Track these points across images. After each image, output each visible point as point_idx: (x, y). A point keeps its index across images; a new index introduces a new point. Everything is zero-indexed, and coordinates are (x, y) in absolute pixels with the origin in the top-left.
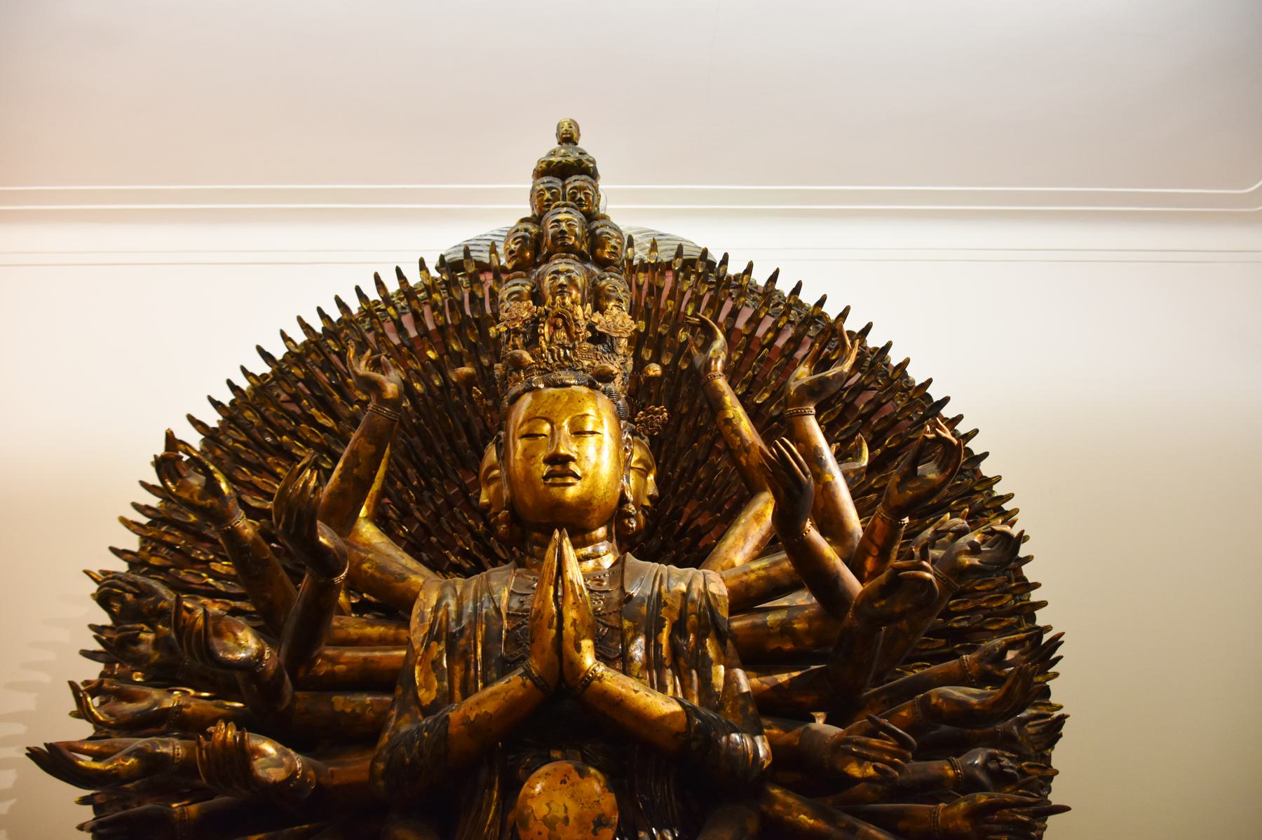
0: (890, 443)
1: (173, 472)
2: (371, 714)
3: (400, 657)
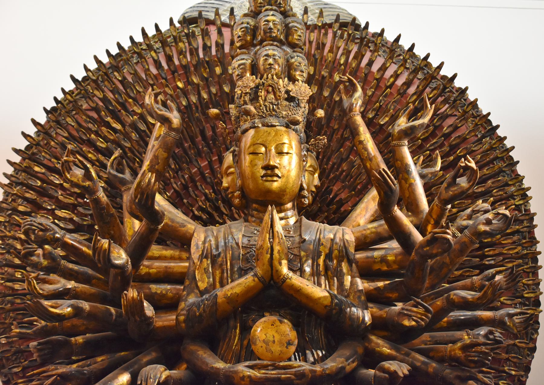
0: (460, 152)
1: (68, 168)
2: (171, 294)
3: (185, 267)
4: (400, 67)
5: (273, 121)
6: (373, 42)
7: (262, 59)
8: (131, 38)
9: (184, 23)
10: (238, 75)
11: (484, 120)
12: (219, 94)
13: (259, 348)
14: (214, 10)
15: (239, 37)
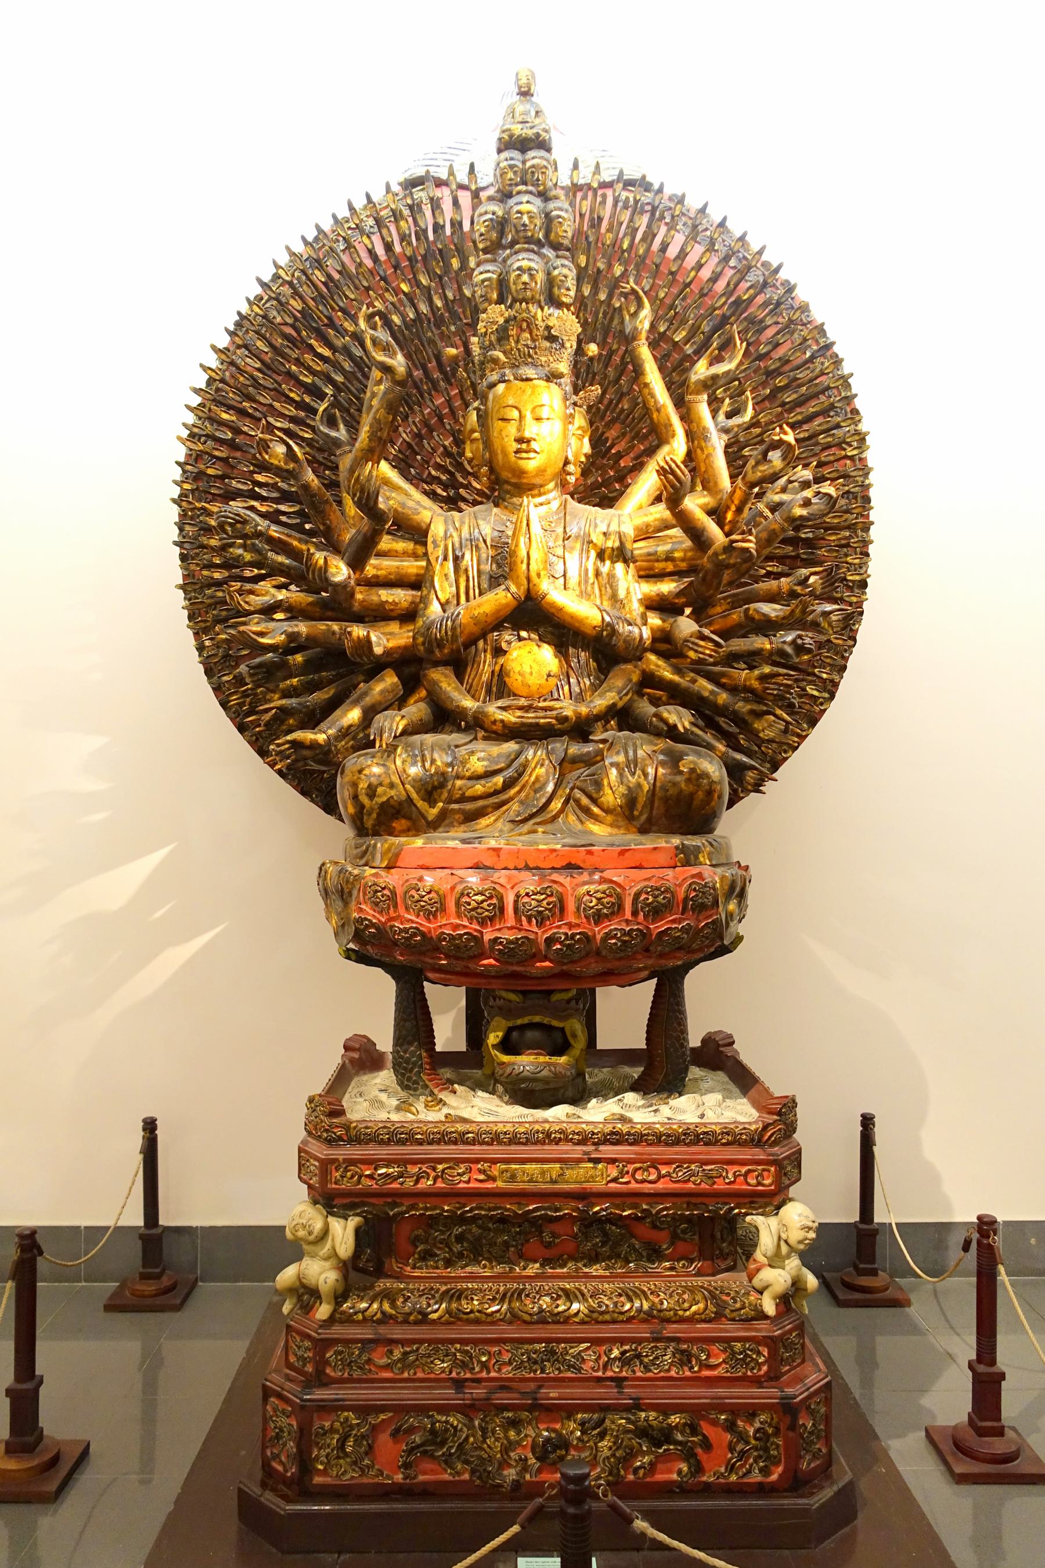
0: (780, 382)
3: (422, 567)
5: (529, 372)
7: (513, 275)
13: (514, 681)
15: (481, 235)
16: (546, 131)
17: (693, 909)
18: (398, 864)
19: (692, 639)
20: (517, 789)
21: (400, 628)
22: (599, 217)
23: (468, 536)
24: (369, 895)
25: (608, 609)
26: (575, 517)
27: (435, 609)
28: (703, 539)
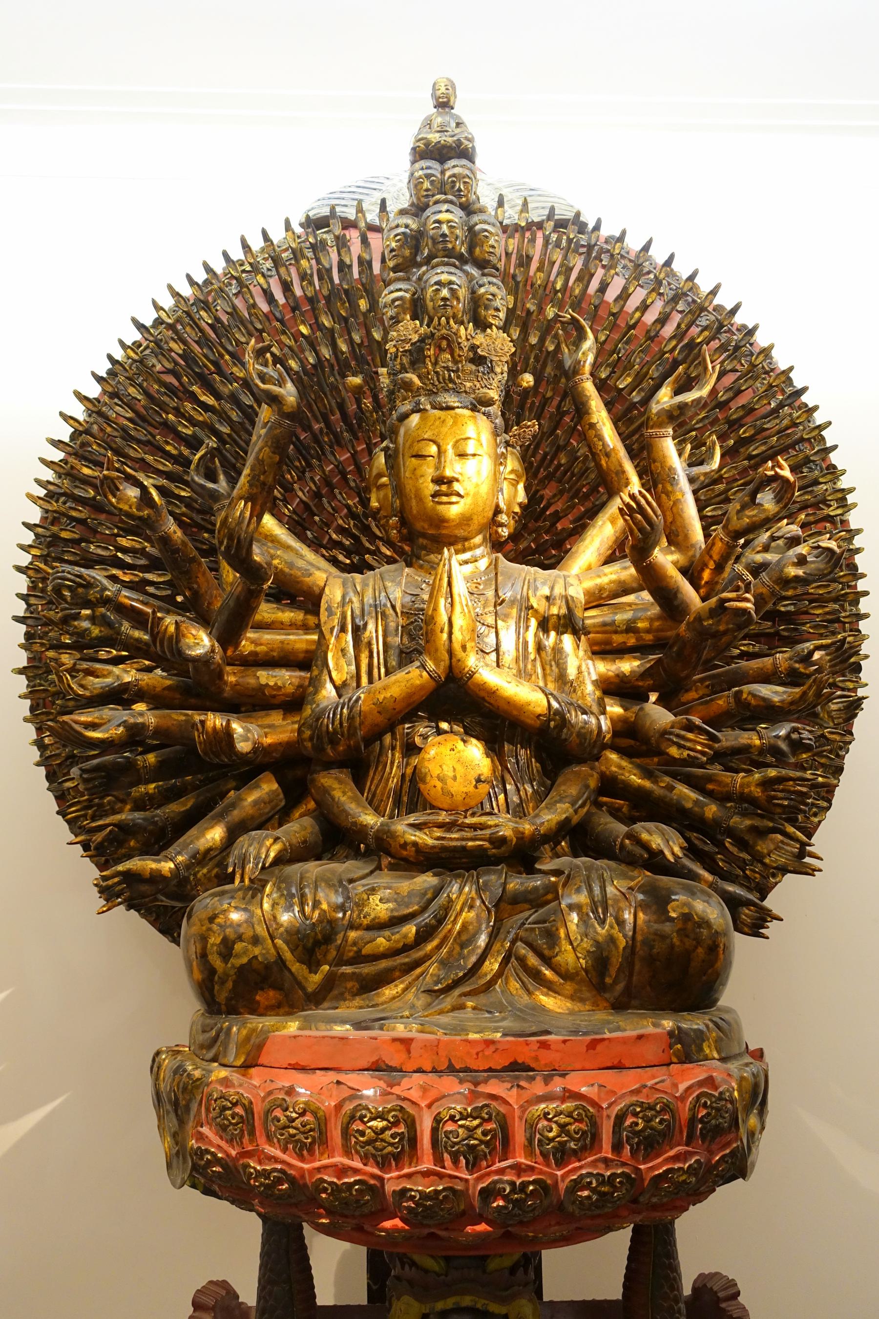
0: (744, 432)
3: (313, 641)
4: (650, 293)
5: (451, 399)
6: (608, 251)
8: (225, 254)
9: (309, 227)
10: (392, 318)
11: (783, 378)
12: (366, 344)
13: (432, 788)
14: (355, 203)
15: (392, 250)
16: (467, 138)
17: (703, 1136)
18: (260, 1061)
19: (677, 731)
20: (435, 943)
21: (284, 719)
22: (527, 256)
23: (371, 601)
24: (213, 1114)
25: (555, 693)
26: (510, 578)
27: (328, 692)
28: (676, 603)
